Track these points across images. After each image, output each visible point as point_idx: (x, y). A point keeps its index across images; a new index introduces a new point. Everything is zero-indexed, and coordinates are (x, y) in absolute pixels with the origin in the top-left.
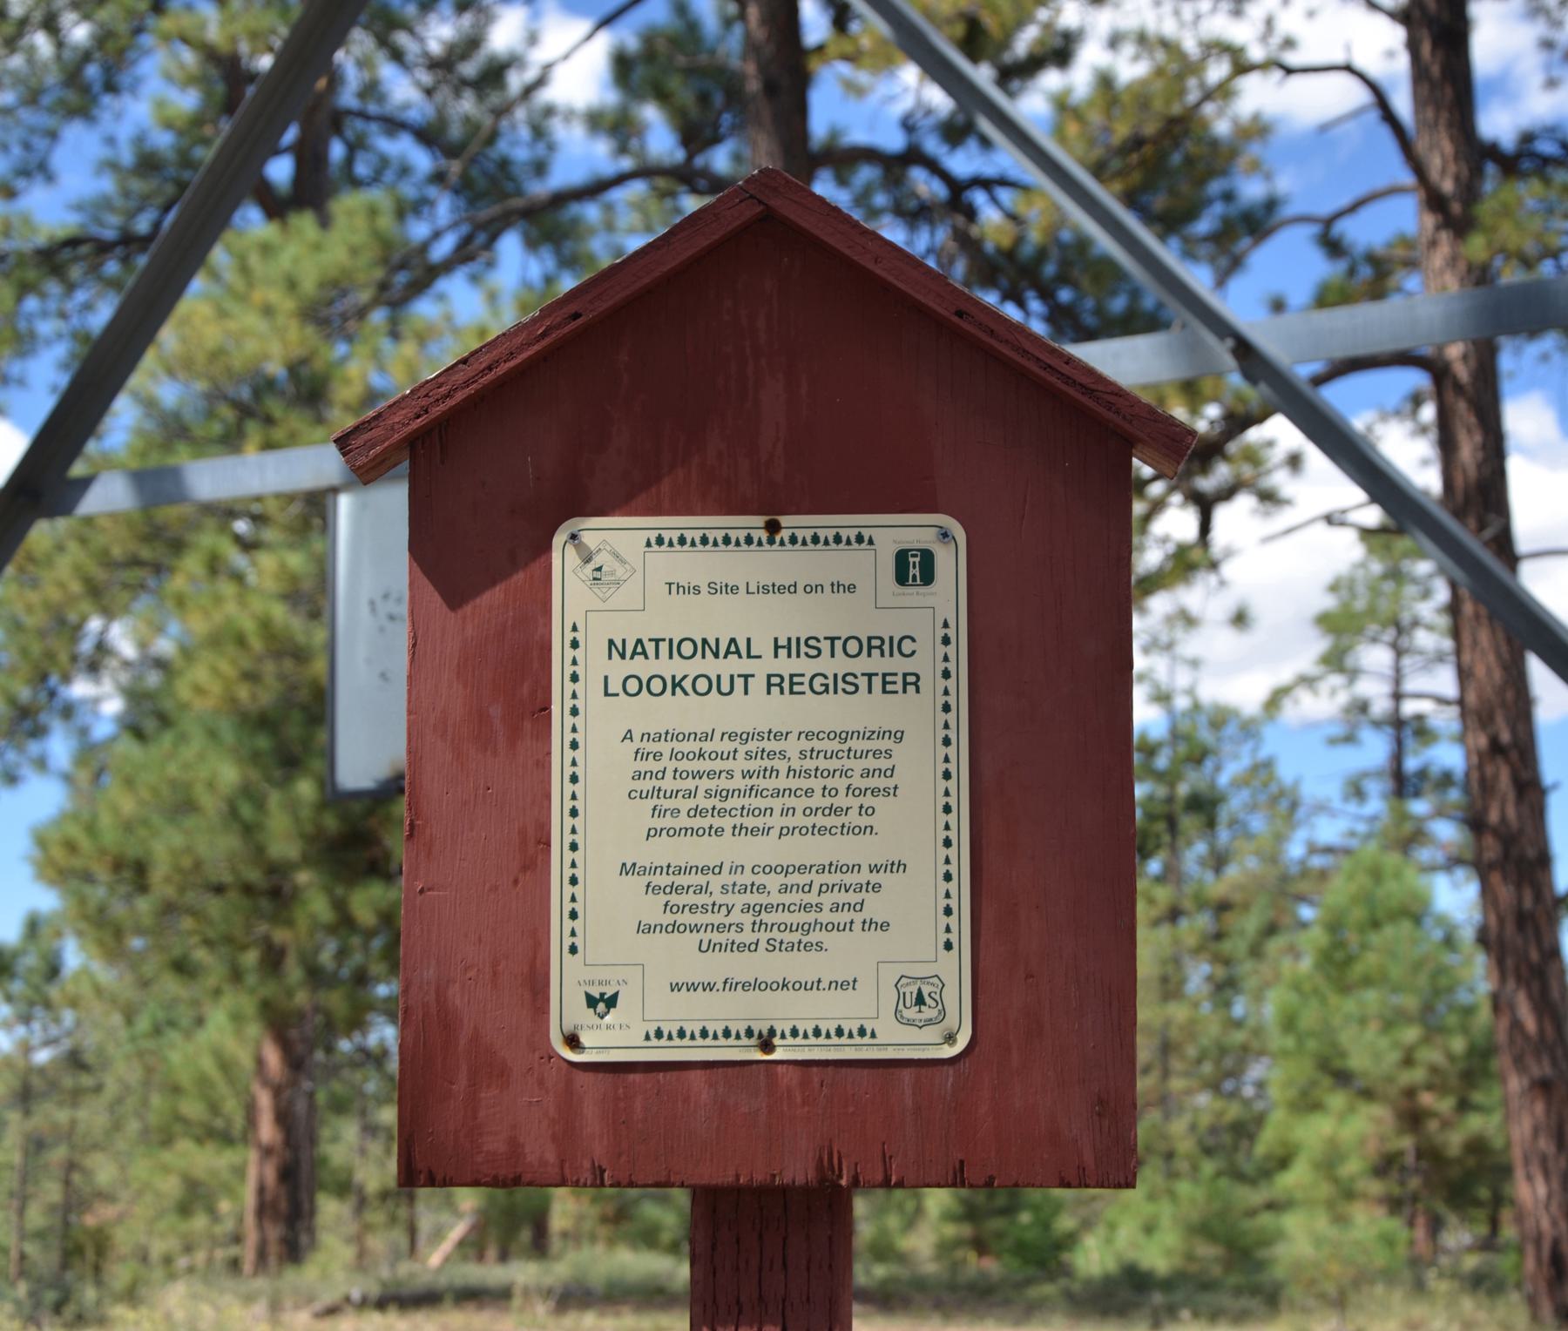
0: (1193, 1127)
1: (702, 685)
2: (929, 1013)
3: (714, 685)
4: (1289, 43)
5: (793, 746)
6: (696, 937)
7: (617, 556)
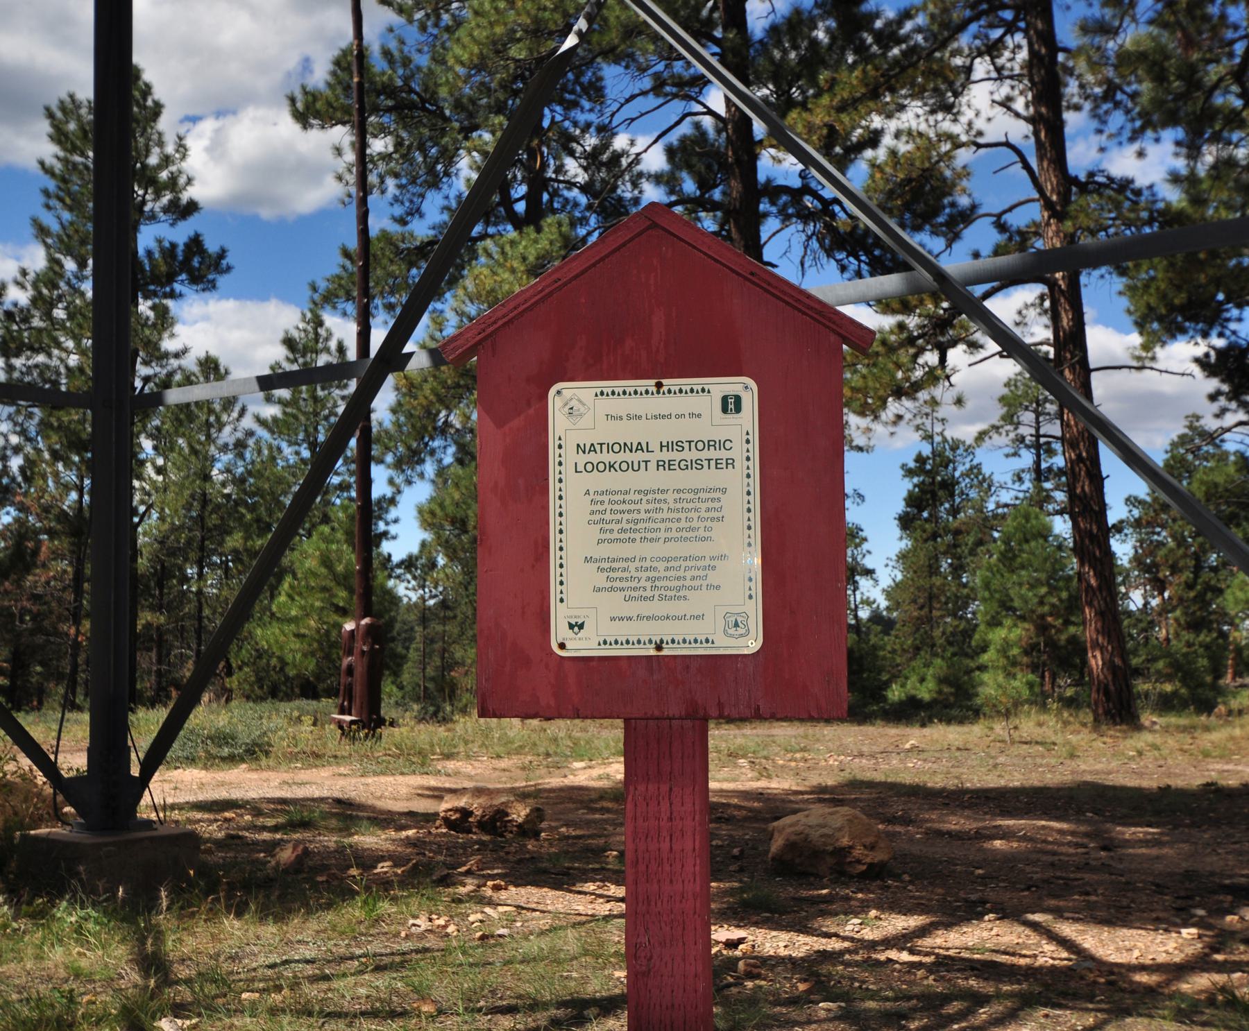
0: (944, 633)
1: (624, 466)
2: (741, 631)
3: (630, 466)
4: (980, 134)
5: (670, 497)
6: (623, 593)
7: (580, 401)
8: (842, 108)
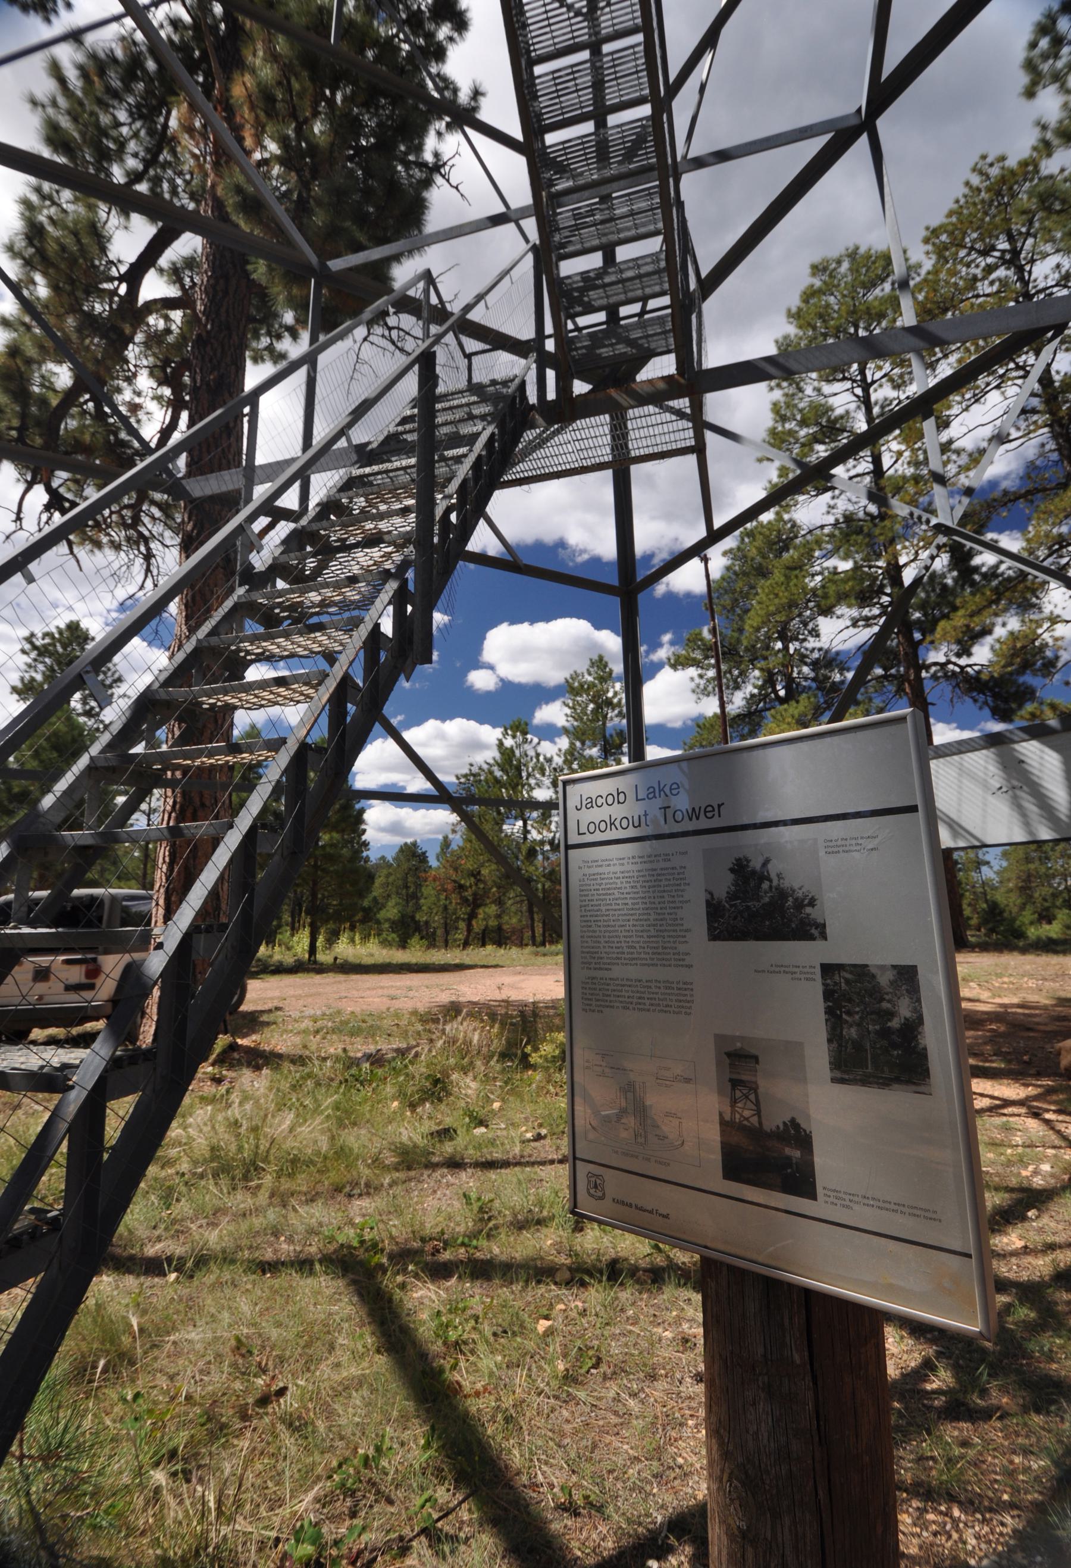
8: (971, 616)
